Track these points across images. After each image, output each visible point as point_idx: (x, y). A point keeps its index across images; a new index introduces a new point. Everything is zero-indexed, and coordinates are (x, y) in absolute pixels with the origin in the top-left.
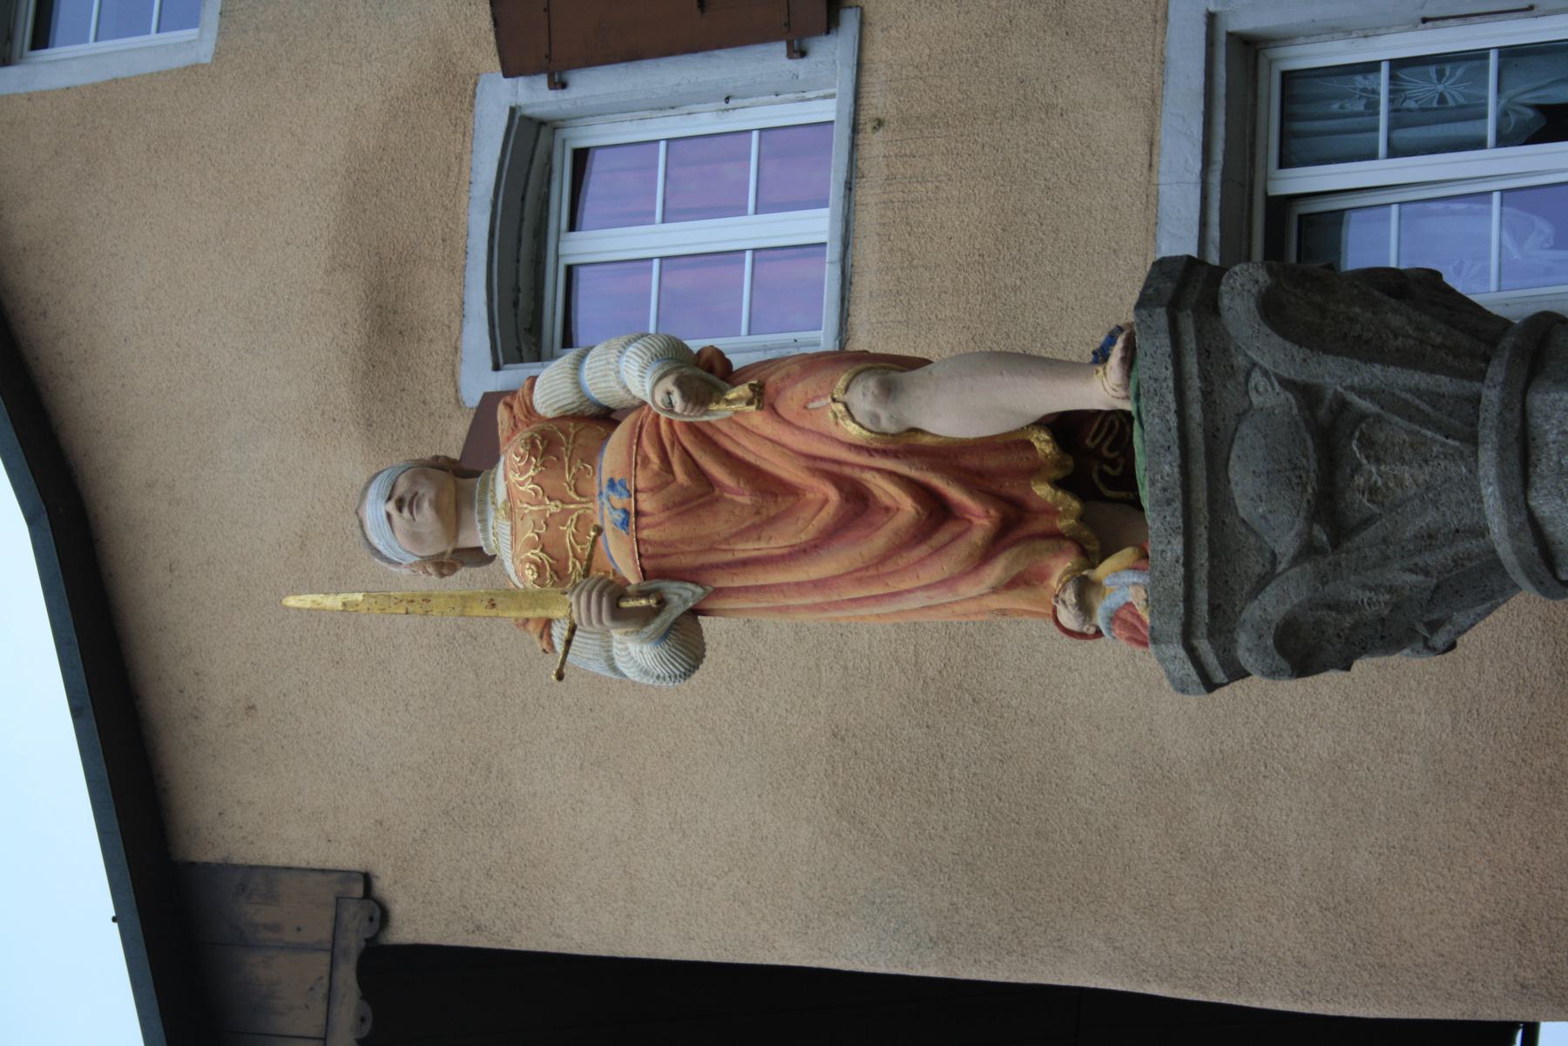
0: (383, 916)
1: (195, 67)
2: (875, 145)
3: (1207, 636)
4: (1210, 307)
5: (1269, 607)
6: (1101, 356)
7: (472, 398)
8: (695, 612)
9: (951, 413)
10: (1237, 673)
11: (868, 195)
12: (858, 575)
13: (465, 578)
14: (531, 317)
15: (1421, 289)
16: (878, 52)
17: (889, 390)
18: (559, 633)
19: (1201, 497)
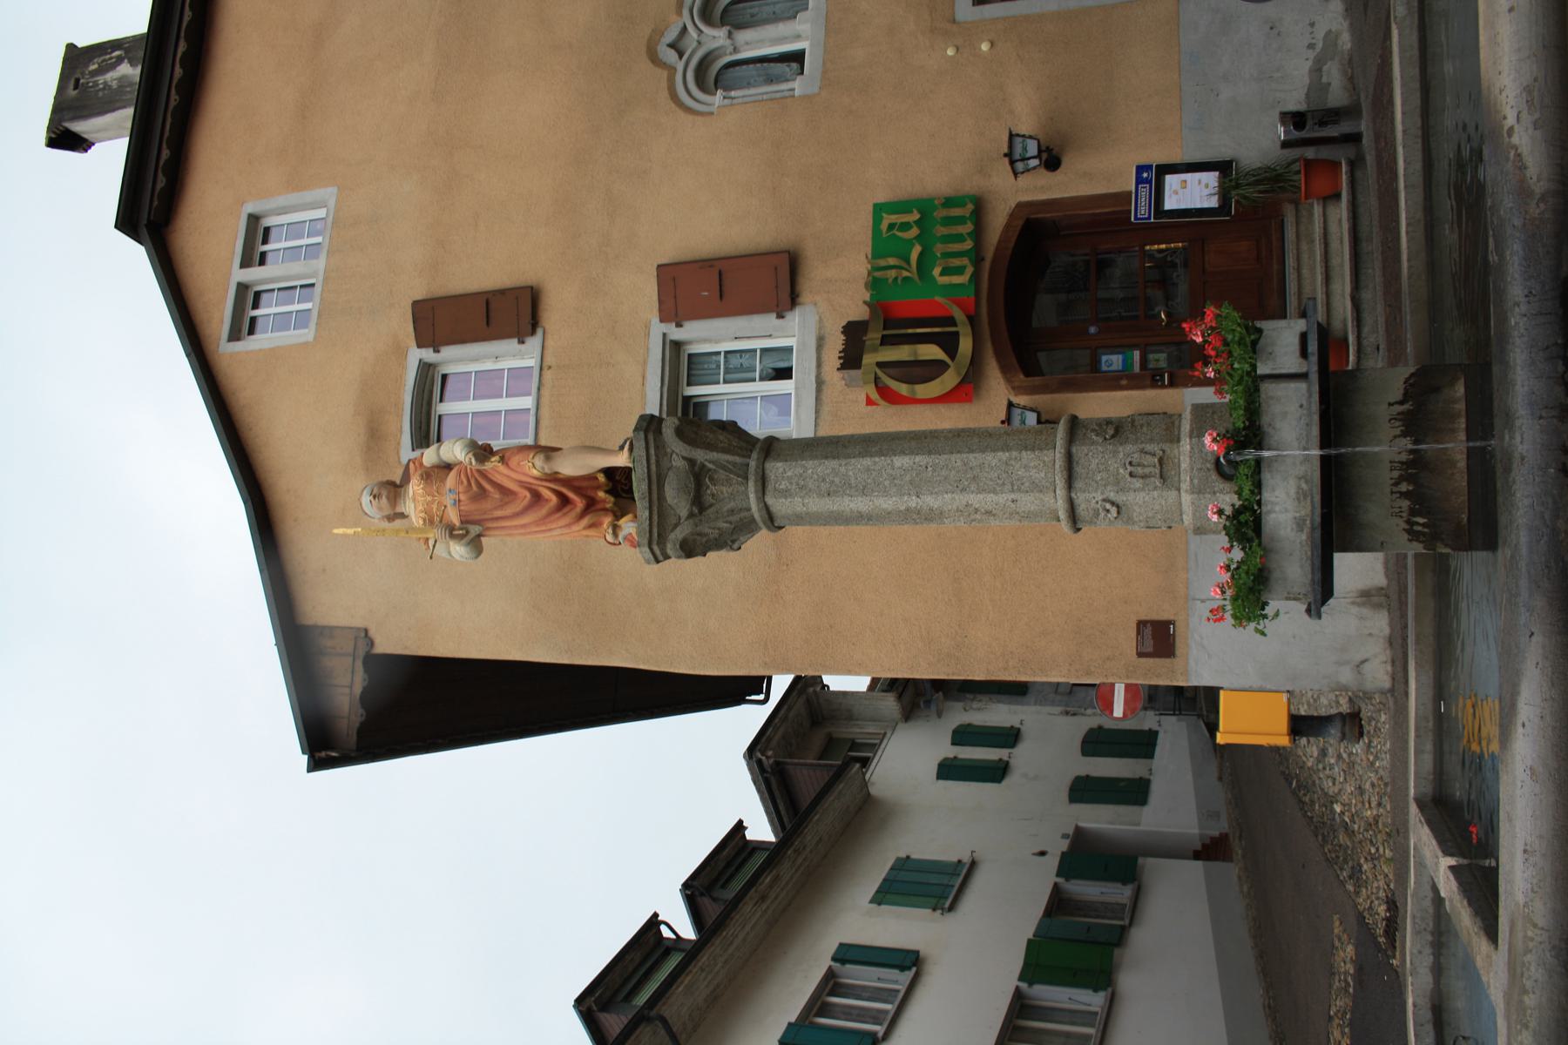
0: (372, 643)
1: (306, 343)
2: (548, 374)
3: (657, 544)
4: (659, 432)
5: (677, 535)
6: (622, 448)
7: (404, 461)
8: (479, 536)
9: (570, 467)
10: (667, 557)
11: (545, 392)
12: (537, 523)
13: (398, 523)
14: (425, 431)
15: (730, 428)
16: (550, 343)
17: (548, 459)
18: (431, 543)
19: (655, 496)
